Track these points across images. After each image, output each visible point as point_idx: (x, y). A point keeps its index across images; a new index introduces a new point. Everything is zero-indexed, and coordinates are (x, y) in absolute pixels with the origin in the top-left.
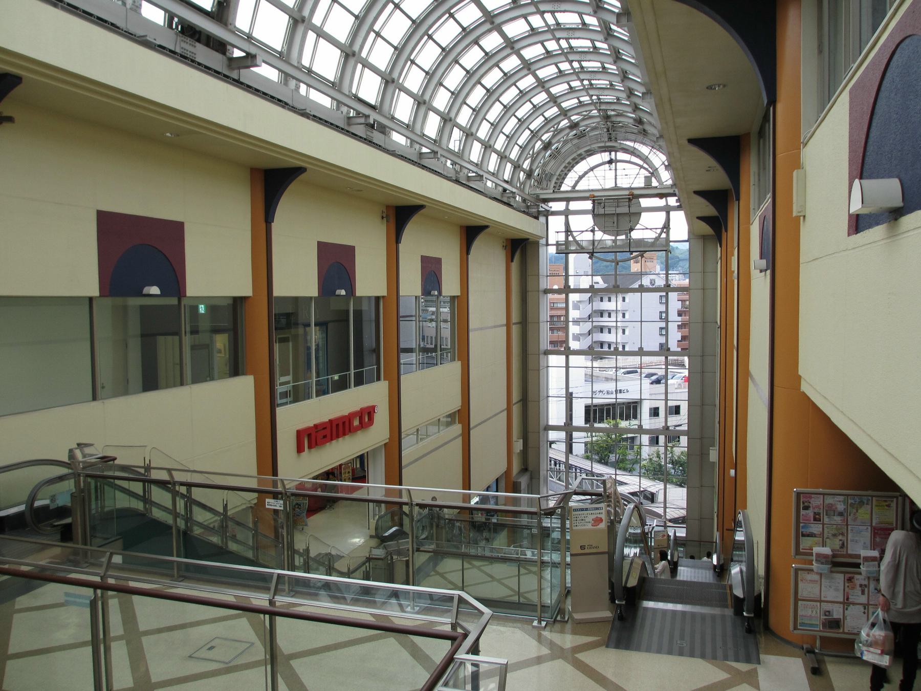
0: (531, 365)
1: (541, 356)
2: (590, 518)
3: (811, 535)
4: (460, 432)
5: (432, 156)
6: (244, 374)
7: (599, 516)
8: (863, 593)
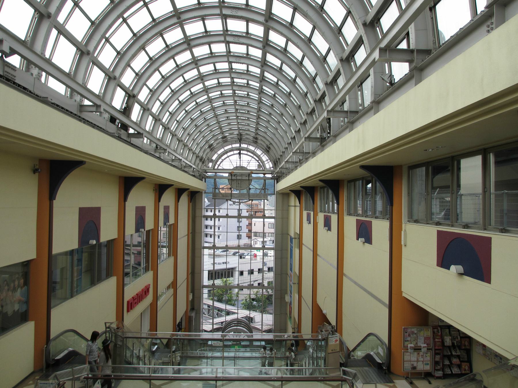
2: (334, 340)
3: (408, 341)
5: (94, 109)
7: (337, 339)
8: (422, 357)
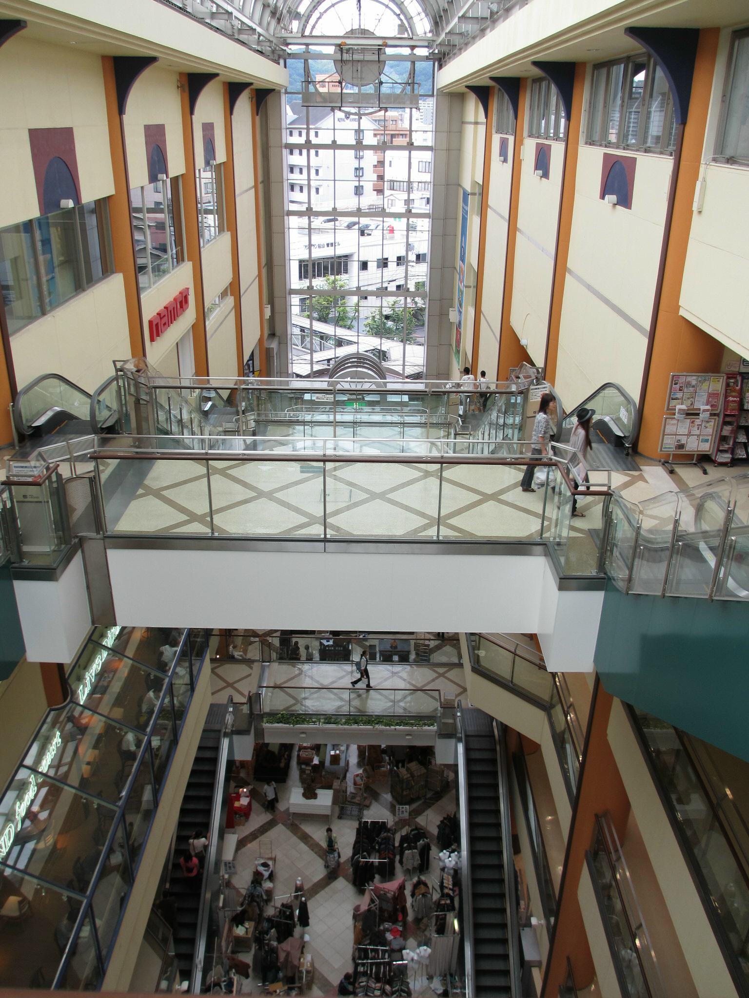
0: (275, 228)
1: (286, 217)
4: (233, 304)
6: (113, 272)
